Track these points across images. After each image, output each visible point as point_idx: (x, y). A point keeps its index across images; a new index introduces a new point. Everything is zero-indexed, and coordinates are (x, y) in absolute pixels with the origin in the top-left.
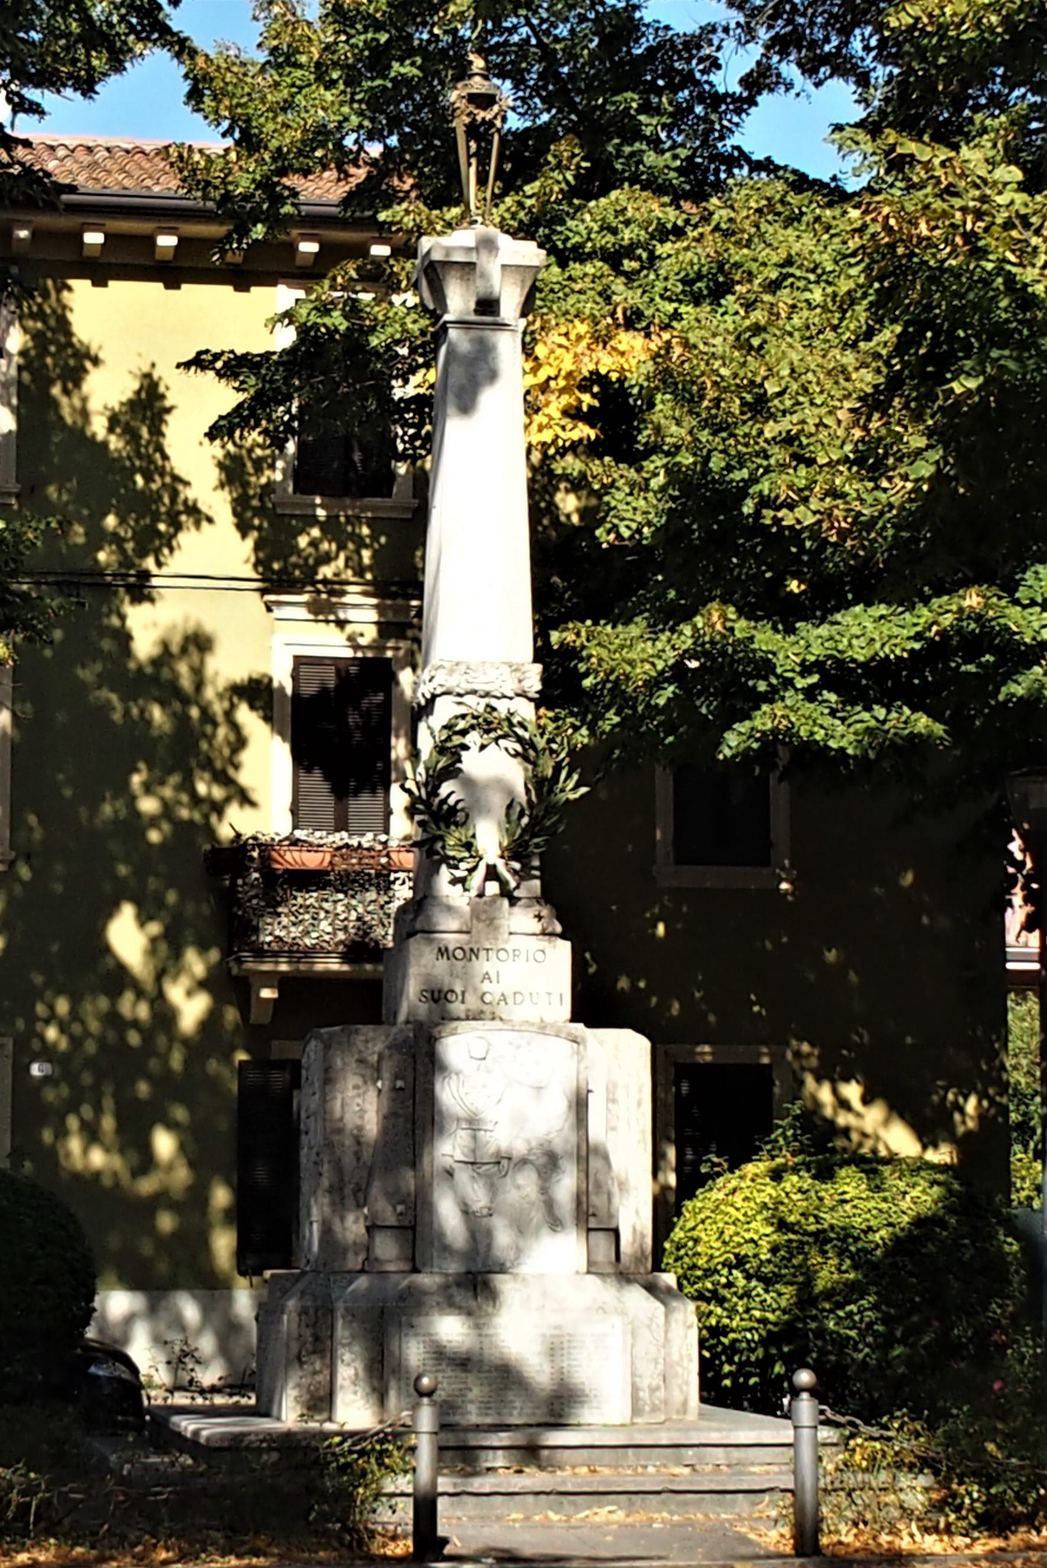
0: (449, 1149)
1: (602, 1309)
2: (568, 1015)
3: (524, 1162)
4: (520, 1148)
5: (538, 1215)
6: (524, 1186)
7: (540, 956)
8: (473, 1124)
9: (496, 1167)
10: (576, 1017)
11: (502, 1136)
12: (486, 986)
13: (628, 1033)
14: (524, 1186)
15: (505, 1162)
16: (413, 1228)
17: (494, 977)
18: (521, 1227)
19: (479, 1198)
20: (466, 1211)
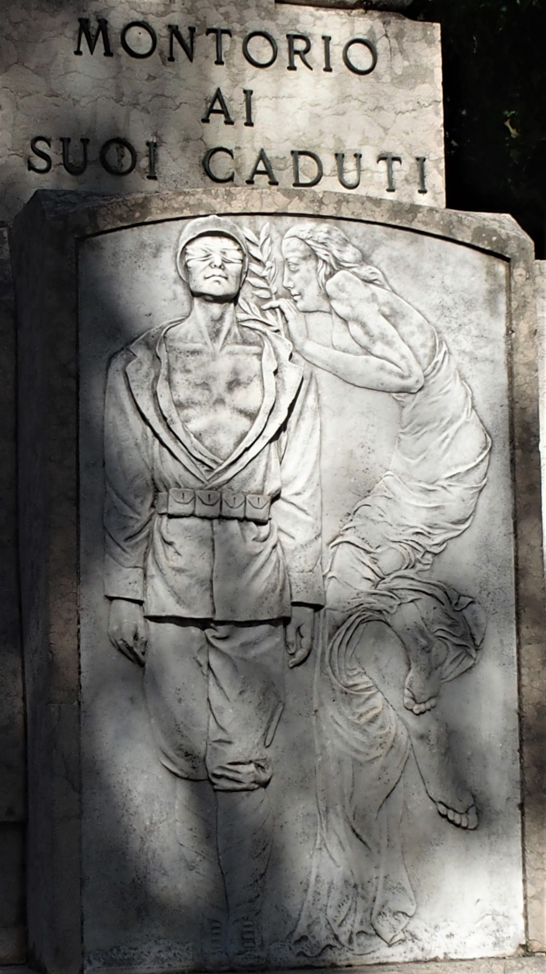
0: (159, 579)
1: (254, 834)
2: (444, 206)
3: (366, 621)
4: (347, 578)
5: (419, 799)
6: (378, 703)
7: (361, 57)
8: (223, 508)
9: (284, 639)
10: (450, 204)
11: (302, 542)
12: (219, 133)
13: (508, 216)
14: (378, 703)
15: (301, 616)
16: (22, 826)
17: (237, 106)
18: (370, 828)
19: (235, 732)
20: (202, 780)
